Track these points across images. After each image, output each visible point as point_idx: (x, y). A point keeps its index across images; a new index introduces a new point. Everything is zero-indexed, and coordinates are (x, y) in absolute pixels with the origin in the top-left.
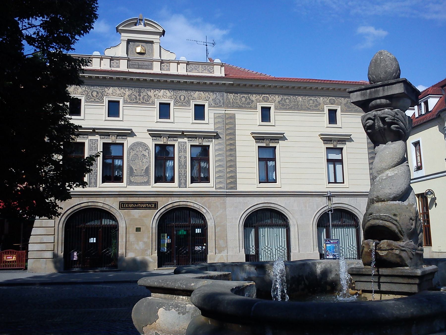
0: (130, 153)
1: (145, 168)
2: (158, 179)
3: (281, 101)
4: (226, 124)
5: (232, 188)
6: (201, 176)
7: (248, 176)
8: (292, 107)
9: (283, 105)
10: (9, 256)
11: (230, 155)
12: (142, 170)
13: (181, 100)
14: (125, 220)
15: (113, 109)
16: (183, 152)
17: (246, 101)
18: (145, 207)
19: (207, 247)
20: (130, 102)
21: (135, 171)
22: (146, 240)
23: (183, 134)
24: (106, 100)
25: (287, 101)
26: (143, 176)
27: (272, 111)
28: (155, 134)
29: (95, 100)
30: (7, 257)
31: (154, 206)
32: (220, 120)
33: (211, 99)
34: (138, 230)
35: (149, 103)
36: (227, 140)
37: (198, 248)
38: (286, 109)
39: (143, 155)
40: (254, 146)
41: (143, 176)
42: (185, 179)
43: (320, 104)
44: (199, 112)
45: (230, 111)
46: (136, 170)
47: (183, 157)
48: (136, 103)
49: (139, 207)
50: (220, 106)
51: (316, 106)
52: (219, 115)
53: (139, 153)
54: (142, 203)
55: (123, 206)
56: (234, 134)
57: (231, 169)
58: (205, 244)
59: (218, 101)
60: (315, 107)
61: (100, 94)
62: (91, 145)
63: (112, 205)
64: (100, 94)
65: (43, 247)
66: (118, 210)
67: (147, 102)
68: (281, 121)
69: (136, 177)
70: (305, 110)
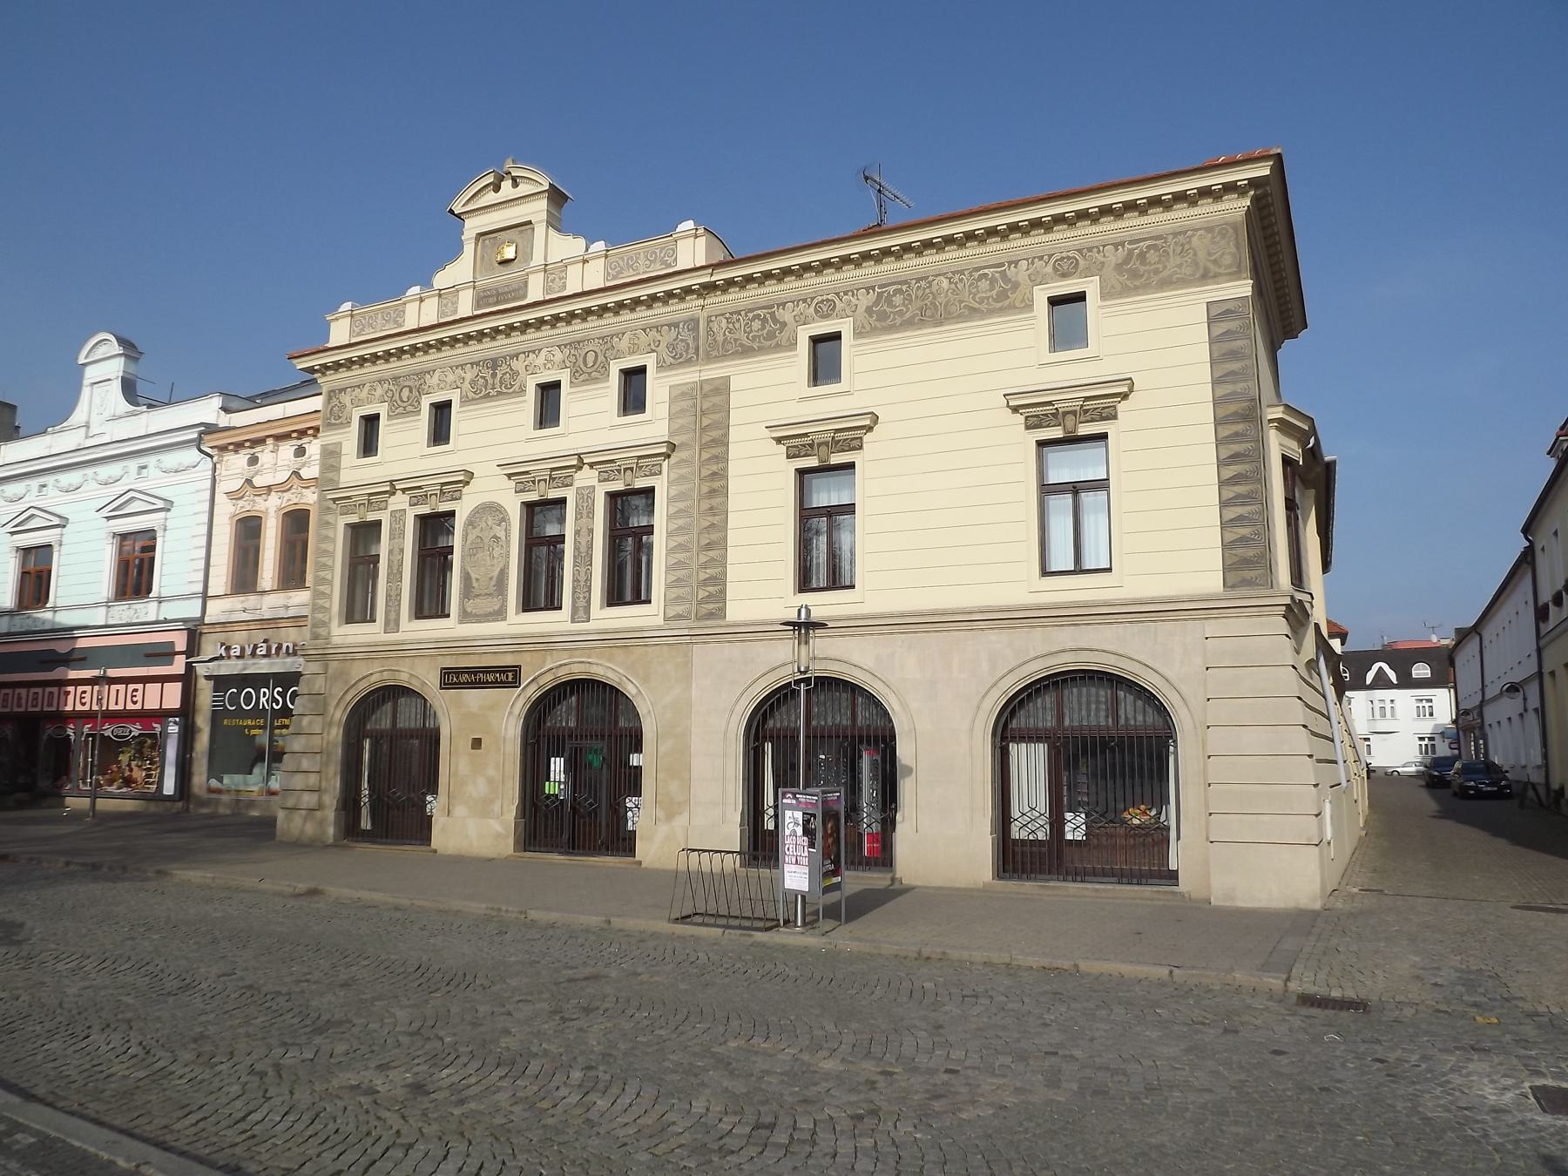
1: (496, 573)
3: (876, 303)
4: (703, 413)
5: (710, 615)
6: (625, 584)
7: (761, 582)
8: (913, 317)
9: (883, 316)
11: (711, 508)
14: (456, 714)
17: (763, 328)
21: (475, 584)
22: (491, 772)
24: (615, 368)
25: (898, 299)
27: (383, 421)
28: (519, 476)
31: (508, 677)
32: (685, 404)
33: (663, 345)
36: (703, 464)
38: (892, 329)
39: (495, 537)
40: (784, 472)
43: (1016, 286)
44: (633, 395)
45: (713, 371)
47: (584, 532)
48: (487, 396)
50: (689, 362)
51: (1003, 295)
52: (684, 389)
56: (723, 442)
57: (711, 553)
60: (996, 301)
61: (415, 393)
63: (425, 678)
64: (415, 393)
70: (960, 318)
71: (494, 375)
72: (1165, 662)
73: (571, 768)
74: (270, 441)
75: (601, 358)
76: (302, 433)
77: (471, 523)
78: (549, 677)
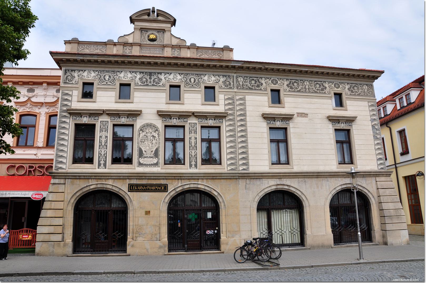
0: (140, 134)
1: (154, 149)
2: (115, 161)
3: (350, 88)
7: (260, 158)
10: (25, 235)
12: (152, 151)
13: (191, 82)
14: (138, 203)
15: (125, 90)
16: (194, 136)
17: (255, 83)
18: (154, 190)
19: (219, 231)
20: (141, 85)
21: (144, 152)
23: (194, 114)
25: (295, 84)
26: (152, 157)
29: (107, 83)
30: (23, 235)
31: (164, 188)
34: (148, 213)
35: (160, 86)
37: (209, 232)
39: (153, 136)
40: (264, 126)
41: (152, 157)
42: (105, 159)
46: (145, 151)
47: (193, 138)
49: (148, 190)
53: (149, 134)
54: (151, 185)
55: (132, 188)
58: (217, 228)
59: (228, 83)
62: (102, 127)
63: (122, 187)
65: (51, 229)
66: (127, 192)
67: (157, 83)
68: (291, 104)
69: (145, 159)
71: (150, 78)
72: (368, 186)
73: (181, 222)
74: (45, 85)
75: (197, 81)
76: (35, 83)
77: (141, 130)
78: (181, 188)
